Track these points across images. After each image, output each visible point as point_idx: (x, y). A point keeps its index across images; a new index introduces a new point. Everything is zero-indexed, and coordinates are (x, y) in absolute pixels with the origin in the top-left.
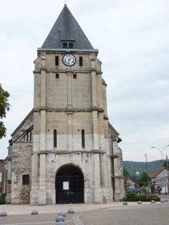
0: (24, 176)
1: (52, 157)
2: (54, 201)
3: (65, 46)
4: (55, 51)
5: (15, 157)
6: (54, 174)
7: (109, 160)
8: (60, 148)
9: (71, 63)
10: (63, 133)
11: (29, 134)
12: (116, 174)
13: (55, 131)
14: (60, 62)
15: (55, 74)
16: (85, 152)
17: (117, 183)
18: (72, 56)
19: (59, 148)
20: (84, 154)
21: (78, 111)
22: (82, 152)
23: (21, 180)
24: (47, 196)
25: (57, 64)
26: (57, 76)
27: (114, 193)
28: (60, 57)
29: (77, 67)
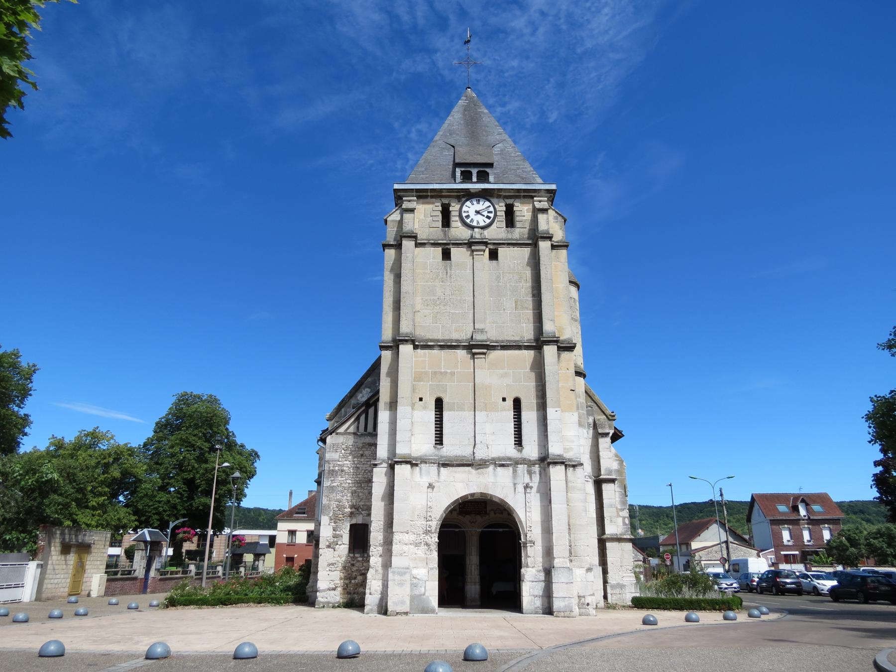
0: (353, 527)
1: (428, 473)
2: (434, 600)
3: (466, 177)
4: (441, 190)
5: (332, 473)
6: (435, 525)
7: (590, 488)
8: (452, 447)
9: (482, 221)
10: (461, 409)
11: (371, 411)
12: (610, 530)
13: (439, 403)
14: (455, 222)
15: (439, 250)
16: (524, 461)
17: (612, 548)
18: (483, 205)
19: (451, 448)
20: (521, 468)
21: (504, 347)
22: (516, 463)
23: (346, 538)
24: (414, 586)
25: (446, 222)
26: (446, 255)
27: (605, 582)
28: (454, 207)
29: (498, 231)
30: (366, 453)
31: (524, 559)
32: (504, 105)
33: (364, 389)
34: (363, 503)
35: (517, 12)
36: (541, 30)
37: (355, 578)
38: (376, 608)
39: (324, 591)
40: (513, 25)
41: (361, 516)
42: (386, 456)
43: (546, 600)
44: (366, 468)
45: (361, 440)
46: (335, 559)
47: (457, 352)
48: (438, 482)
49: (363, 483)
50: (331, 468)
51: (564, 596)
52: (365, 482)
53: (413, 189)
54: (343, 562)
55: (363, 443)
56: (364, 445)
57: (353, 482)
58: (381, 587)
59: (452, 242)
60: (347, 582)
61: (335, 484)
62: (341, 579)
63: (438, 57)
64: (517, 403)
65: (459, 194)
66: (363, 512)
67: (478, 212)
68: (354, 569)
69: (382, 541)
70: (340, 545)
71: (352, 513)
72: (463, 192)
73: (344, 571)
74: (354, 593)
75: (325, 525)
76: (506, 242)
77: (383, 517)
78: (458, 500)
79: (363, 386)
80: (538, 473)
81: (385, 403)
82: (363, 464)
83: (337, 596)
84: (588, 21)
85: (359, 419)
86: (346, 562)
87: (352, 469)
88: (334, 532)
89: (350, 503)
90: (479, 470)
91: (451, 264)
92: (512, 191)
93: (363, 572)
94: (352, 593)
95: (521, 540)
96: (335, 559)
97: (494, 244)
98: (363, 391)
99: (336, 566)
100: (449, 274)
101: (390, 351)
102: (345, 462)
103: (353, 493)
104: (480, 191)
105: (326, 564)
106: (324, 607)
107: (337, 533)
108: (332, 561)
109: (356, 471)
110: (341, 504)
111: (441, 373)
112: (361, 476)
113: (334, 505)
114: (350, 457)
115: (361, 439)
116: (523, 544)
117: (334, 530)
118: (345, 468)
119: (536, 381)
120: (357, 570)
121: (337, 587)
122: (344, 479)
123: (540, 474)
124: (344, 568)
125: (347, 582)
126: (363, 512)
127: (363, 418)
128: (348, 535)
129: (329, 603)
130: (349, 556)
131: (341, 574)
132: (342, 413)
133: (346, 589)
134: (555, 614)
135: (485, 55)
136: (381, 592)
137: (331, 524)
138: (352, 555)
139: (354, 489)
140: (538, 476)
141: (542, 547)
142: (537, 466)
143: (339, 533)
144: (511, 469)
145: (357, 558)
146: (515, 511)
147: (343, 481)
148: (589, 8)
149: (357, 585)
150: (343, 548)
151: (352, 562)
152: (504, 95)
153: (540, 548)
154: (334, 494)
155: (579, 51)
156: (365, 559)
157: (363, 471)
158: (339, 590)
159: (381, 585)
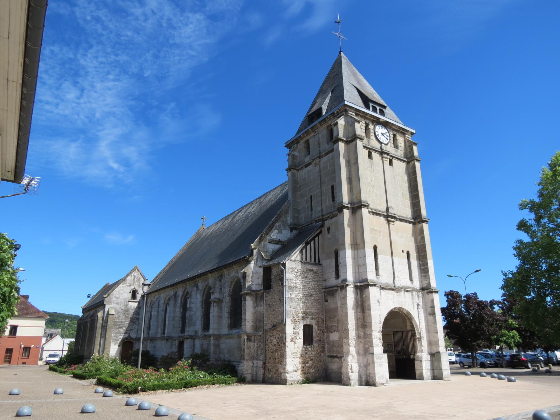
30: (309, 276)
31: (419, 348)
32: (117, 55)
33: (274, 230)
34: (309, 311)
35: (137, 5)
36: (150, 21)
37: (308, 363)
38: (357, 382)
39: (291, 372)
40: (133, 11)
41: (309, 319)
42: (352, 280)
43: (432, 371)
44: (309, 286)
45: (305, 266)
46: (296, 350)
47: (380, 218)
48: (381, 299)
49: (308, 296)
50: (290, 285)
51: (446, 369)
52: (309, 296)
53: (354, 108)
54: (300, 352)
55: (307, 269)
56: (307, 270)
57: (303, 295)
58: (358, 367)
59: (374, 148)
60: (303, 365)
61: (293, 296)
62: (300, 363)
63: (77, 9)
64: (408, 253)
65: (374, 119)
66: (309, 317)
67: (383, 134)
68: (307, 356)
69: (355, 337)
70: (298, 339)
71: (303, 317)
72: (377, 119)
73: (301, 358)
74: (308, 373)
75: (289, 325)
76: (397, 157)
77: (354, 321)
78: (389, 312)
79: (274, 228)
80: (421, 297)
81: (349, 245)
82: (308, 283)
83: (298, 376)
84: (180, 28)
85: (302, 252)
86: (302, 351)
87: (301, 286)
88: (294, 330)
89: (302, 310)
90: (398, 293)
91: (373, 162)
92: (398, 127)
93: (312, 358)
94: (307, 373)
95: (416, 336)
96: (296, 350)
97: (391, 156)
98: (274, 231)
99: (297, 354)
100: (372, 168)
101: (348, 211)
102: (297, 281)
103: (303, 303)
104: (383, 122)
105: (291, 353)
106: (292, 384)
107: (296, 331)
108: (293, 351)
109: (304, 288)
110: (297, 310)
111: (375, 229)
112: (306, 292)
113: (293, 310)
114: (300, 278)
115: (305, 266)
116: (418, 339)
117: (294, 329)
118: (298, 285)
119: (415, 243)
120: (308, 357)
121: (298, 369)
122: (298, 293)
123: (422, 298)
124: (301, 355)
125: (303, 365)
126: (309, 317)
127: (304, 251)
128: (302, 332)
129: (294, 381)
130: (304, 347)
131: (300, 360)
132: (261, 245)
133: (303, 371)
134: (444, 379)
135: (110, 21)
136: (358, 371)
137: (292, 324)
138: (305, 347)
139: (304, 300)
140: (421, 298)
141: (427, 340)
142: (421, 293)
143: (297, 331)
144: (410, 293)
145: (308, 348)
146: (414, 319)
147: (297, 294)
148: (181, 21)
149: (309, 367)
150: (300, 341)
151: (305, 351)
152: (118, 50)
153: (426, 341)
154: (293, 304)
155: (171, 42)
156: (312, 349)
157: (308, 288)
158: (299, 371)
159: (358, 366)
